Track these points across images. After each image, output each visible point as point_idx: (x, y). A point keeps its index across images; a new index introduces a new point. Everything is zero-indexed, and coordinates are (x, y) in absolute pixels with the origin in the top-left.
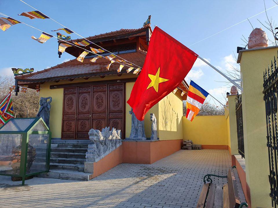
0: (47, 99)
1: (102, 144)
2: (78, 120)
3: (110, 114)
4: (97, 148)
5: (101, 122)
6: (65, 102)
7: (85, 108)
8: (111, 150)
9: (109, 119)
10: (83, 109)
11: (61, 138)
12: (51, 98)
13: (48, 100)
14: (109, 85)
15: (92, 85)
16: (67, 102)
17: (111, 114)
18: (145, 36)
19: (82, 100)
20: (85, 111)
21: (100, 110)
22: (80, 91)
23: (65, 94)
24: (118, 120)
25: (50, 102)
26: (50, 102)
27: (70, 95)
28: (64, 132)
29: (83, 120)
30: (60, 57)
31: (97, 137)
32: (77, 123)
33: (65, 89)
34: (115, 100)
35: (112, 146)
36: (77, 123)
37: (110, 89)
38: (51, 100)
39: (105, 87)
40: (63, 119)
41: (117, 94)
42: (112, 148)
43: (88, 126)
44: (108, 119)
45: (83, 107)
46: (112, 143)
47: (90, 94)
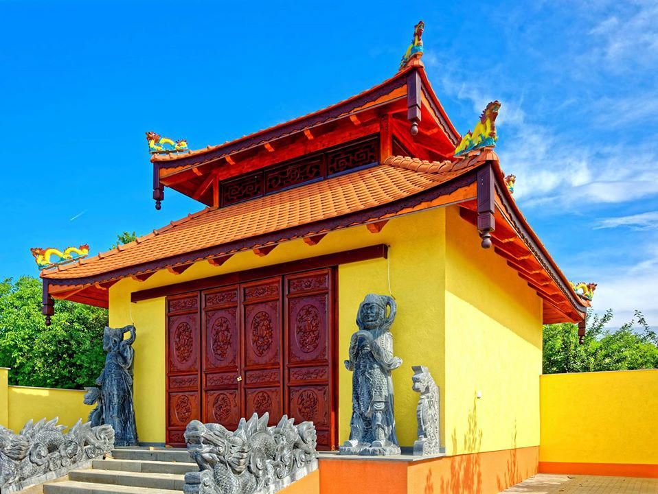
0: (123, 331)
1: (235, 472)
2: (206, 391)
3: (247, 373)
4: (218, 482)
5: (268, 396)
6: (172, 341)
7: (222, 355)
8: (272, 487)
9: (289, 387)
10: (219, 357)
11: (164, 442)
12: (132, 330)
13: (127, 336)
14: (202, 294)
15: (201, 291)
16: (177, 340)
17: (296, 370)
18: (401, 102)
19: (214, 332)
20: (223, 364)
21: (262, 360)
22: (292, 290)
23: (169, 317)
24: (316, 391)
25: (130, 342)
26: (130, 342)
27: (260, 306)
28: (173, 426)
29: (222, 392)
30: (158, 208)
31: (212, 447)
32: (286, 397)
33: (169, 301)
34: (305, 326)
35: (278, 476)
36: (286, 397)
37: (292, 290)
38: (134, 336)
39: (277, 285)
40: (169, 388)
41: (312, 307)
42: (278, 482)
43: (234, 410)
44: (286, 388)
45: (219, 352)
46: (278, 466)
47: (235, 313)
